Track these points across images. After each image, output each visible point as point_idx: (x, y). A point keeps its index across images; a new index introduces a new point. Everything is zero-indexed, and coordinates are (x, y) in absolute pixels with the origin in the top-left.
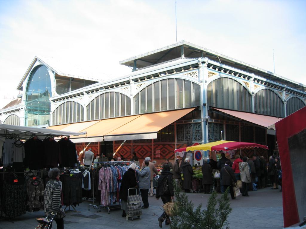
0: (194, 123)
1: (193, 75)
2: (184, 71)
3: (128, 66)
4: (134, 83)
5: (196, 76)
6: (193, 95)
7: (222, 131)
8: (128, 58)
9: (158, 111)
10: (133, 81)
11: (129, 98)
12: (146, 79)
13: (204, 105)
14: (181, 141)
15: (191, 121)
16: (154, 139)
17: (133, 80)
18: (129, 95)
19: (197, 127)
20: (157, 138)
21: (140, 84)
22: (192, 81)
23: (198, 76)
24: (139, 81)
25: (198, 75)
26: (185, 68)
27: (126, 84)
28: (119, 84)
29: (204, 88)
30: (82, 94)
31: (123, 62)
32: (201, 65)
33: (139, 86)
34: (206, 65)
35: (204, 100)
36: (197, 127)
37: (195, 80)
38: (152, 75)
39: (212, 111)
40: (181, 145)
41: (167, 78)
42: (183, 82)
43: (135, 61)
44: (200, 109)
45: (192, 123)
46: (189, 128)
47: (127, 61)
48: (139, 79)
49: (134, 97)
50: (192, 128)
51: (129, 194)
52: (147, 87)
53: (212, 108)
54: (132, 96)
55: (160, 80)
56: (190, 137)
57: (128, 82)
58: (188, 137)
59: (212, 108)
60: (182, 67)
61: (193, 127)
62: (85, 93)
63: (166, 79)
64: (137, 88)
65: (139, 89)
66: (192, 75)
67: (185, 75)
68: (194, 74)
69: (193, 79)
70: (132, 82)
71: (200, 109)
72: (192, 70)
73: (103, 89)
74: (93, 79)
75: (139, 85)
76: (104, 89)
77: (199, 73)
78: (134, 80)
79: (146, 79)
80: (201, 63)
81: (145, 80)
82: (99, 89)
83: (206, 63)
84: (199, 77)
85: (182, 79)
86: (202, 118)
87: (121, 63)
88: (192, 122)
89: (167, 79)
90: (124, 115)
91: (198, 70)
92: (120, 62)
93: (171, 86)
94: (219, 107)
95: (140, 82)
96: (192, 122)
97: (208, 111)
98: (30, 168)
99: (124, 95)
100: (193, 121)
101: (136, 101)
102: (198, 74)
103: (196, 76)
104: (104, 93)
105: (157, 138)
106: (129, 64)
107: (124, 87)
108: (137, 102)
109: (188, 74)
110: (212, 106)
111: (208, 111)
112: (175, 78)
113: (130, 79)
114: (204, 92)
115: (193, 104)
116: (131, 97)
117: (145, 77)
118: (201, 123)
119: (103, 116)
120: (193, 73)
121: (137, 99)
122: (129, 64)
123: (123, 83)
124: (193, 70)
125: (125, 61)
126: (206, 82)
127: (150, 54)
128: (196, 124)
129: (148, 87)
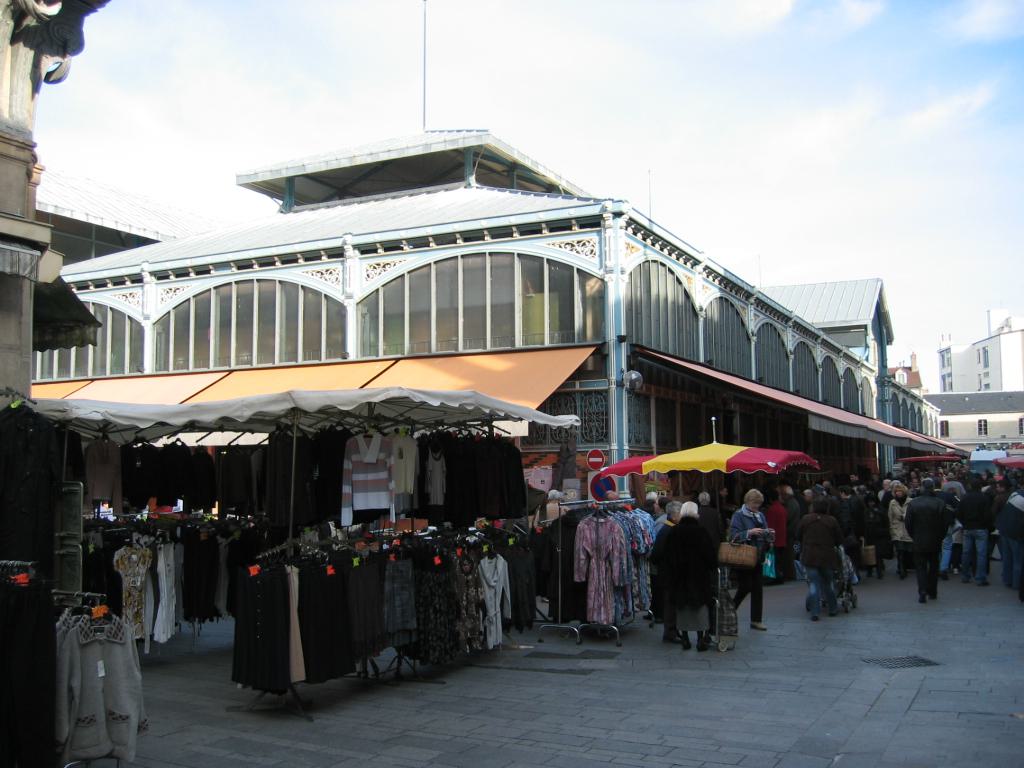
0: (581, 392)
1: (327, 276)
2: (463, 244)
3: (272, 196)
4: (361, 259)
5: (592, 251)
6: (578, 307)
7: (713, 418)
8: (274, 168)
9: (397, 353)
10: (153, 278)
11: (138, 324)
12: (192, 275)
13: (621, 339)
14: (597, 441)
15: (575, 386)
16: (523, 438)
17: (153, 274)
18: (138, 317)
19: (594, 402)
20: (526, 434)
21: (173, 286)
22: (324, 293)
23: (598, 253)
24: (380, 251)
25: (597, 249)
26: (467, 236)
27: (128, 283)
28: (299, 256)
29: (618, 291)
30: (137, 279)
31: (250, 181)
32: (609, 221)
33: (171, 294)
34: (622, 221)
35: (616, 325)
36: (594, 402)
37: (590, 264)
38: (546, 222)
39: (638, 356)
40: (537, 456)
41: (255, 278)
42: (301, 293)
43: (290, 180)
44: (606, 352)
45: (575, 392)
46: (563, 405)
47: (268, 177)
48: (378, 245)
49: (358, 304)
50: (576, 407)
51: (562, 618)
52: (409, 272)
53: (637, 349)
54: (147, 318)
55: (487, 251)
56: (597, 431)
57: (337, 253)
58: (591, 431)
59: (637, 349)
60: (431, 236)
61: (578, 404)
62: (147, 278)
63: (485, 253)
64: (165, 296)
65: (169, 300)
66: (577, 247)
67: (551, 246)
68: (584, 244)
69: (328, 287)
70: (350, 252)
71: (606, 352)
72: (577, 235)
73: (231, 267)
74: (130, 226)
75: (378, 265)
76: (234, 270)
77: (600, 243)
78: (155, 276)
79: (192, 275)
80: (611, 215)
81: (541, 233)
82: (211, 267)
83: (625, 218)
84: (600, 256)
85: (543, 258)
86: (613, 378)
87: (241, 183)
88: (578, 387)
89: (459, 258)
90: (188, 368)
91: (343, 265)
92: (238, 176)
93: (474, 276)
94: (671, 352)
95: (383, 258)
96: (578, 387)
97: (628, 357)
98: (199, 618)
99: (122, 315)
100: (580, 386)
101: (158, 334)
102: (341, 274)
103: (592, 251)
104: (459, 254)
105: (526, 434)
106: (270, 188)
107: (374, 261)
108: (163, 335)
109: (563, 245)
110: (640, 343)
111: (628, 357)
112: (278, 279)
113: (142, 270)
114: (617, 304)
115: (579, 335)
116: (346, 303)
117: (170, 272)
118: (607, 391)
119: (104, 367)
120: (578, 242)
121: (163, 329)
122: (270, 188)
123: (374, 248)
124: (462, 247)
125: (260, 175)
126: (623, 272)
127: (359, 161)
128: (589, 393)
129: (413, 274)
